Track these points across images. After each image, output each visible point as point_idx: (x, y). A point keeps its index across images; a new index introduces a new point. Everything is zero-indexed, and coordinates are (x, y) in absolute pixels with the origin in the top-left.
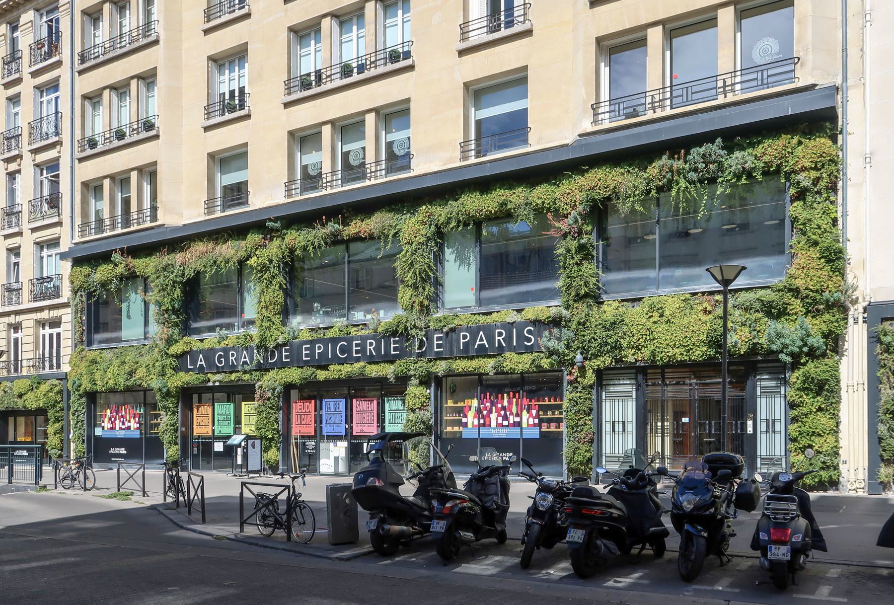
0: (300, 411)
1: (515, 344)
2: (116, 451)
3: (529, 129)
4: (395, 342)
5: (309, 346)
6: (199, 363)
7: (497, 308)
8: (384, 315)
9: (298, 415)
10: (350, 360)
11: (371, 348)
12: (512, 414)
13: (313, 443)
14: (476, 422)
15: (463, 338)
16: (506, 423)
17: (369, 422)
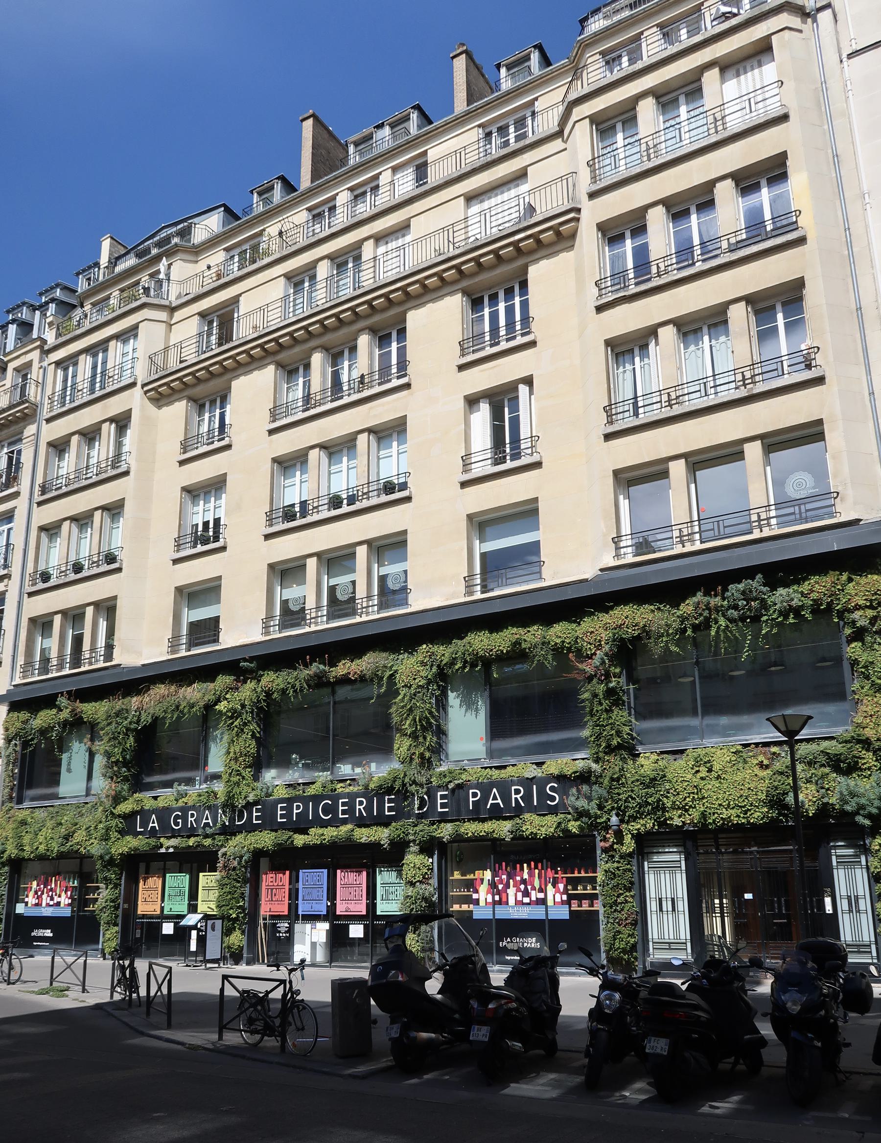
0: (272, 884)
1: (535, 804)
3: (542, 563)
4: (390, 801)
6: (151, 825)
9: (268, 889)
10: (335, 822)
12: (534, 888)
13: (287, 925)
14: (490, 899)
16: (526, 900)
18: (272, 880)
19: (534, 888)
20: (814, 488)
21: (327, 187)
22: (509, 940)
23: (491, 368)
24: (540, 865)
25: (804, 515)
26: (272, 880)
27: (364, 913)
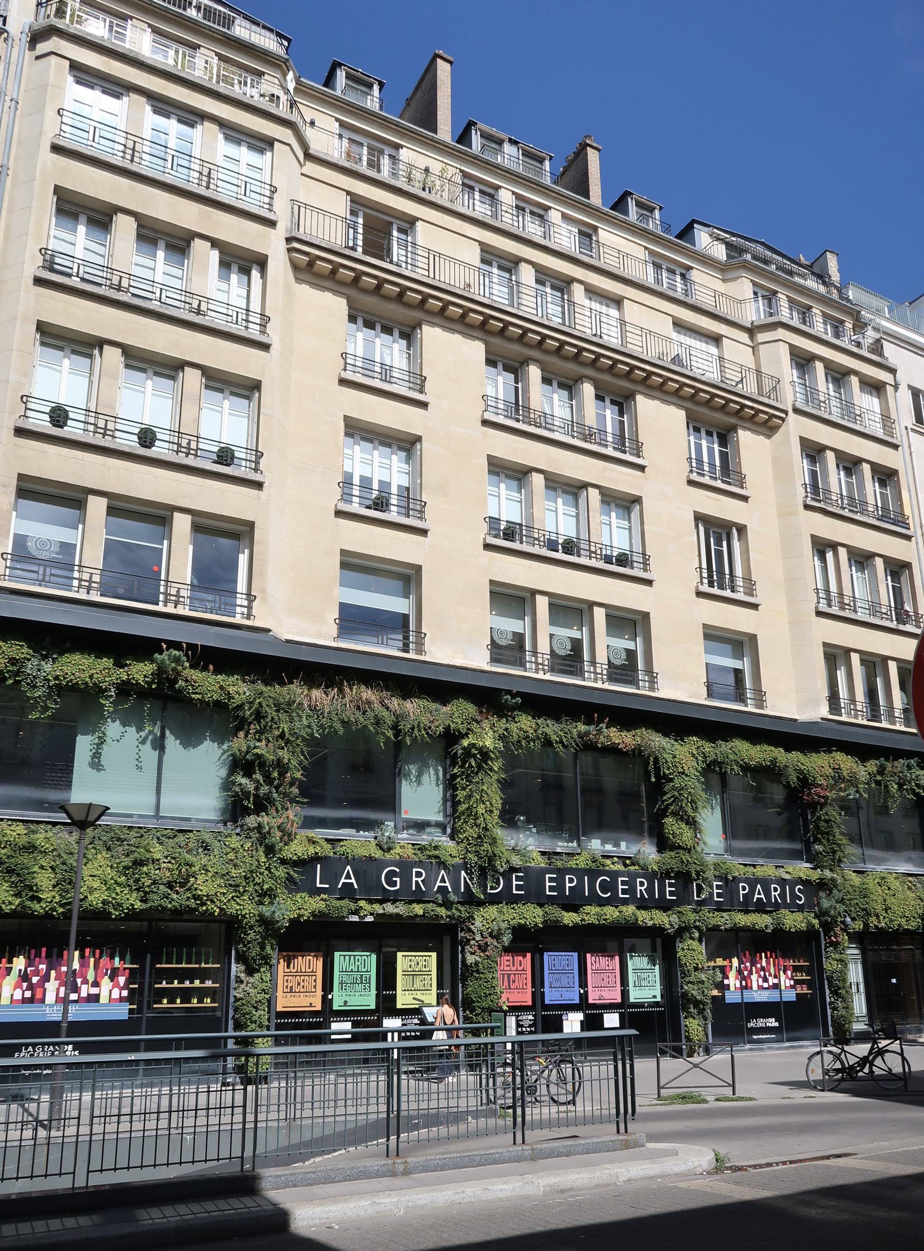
0: (508, 968)
2: (761, 1023)
3: (423, 635)
5: (555, 876)
6: (756, 896)
7: (760, 861)
8: (627, 848)
9: (503, 975)
10: (614, 901)
11: (643, 888)
12: (85, 982)
13: (531, 1017)
14: (738, 985)
15: (743, 890)
16: (766, 985)
17: (651, 984)
18: (508, 963)
19: (770, 975)
20: (57, 553)
21: (491, 170)
22: (754, 1021)
23: (716, 499)
24: (774, 954)
25: (47, 578)
26: (508, 963)
27: (373, 1007)
